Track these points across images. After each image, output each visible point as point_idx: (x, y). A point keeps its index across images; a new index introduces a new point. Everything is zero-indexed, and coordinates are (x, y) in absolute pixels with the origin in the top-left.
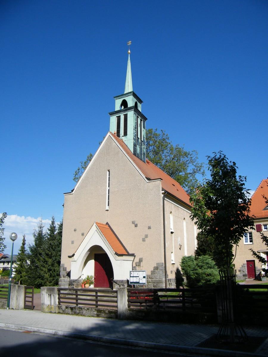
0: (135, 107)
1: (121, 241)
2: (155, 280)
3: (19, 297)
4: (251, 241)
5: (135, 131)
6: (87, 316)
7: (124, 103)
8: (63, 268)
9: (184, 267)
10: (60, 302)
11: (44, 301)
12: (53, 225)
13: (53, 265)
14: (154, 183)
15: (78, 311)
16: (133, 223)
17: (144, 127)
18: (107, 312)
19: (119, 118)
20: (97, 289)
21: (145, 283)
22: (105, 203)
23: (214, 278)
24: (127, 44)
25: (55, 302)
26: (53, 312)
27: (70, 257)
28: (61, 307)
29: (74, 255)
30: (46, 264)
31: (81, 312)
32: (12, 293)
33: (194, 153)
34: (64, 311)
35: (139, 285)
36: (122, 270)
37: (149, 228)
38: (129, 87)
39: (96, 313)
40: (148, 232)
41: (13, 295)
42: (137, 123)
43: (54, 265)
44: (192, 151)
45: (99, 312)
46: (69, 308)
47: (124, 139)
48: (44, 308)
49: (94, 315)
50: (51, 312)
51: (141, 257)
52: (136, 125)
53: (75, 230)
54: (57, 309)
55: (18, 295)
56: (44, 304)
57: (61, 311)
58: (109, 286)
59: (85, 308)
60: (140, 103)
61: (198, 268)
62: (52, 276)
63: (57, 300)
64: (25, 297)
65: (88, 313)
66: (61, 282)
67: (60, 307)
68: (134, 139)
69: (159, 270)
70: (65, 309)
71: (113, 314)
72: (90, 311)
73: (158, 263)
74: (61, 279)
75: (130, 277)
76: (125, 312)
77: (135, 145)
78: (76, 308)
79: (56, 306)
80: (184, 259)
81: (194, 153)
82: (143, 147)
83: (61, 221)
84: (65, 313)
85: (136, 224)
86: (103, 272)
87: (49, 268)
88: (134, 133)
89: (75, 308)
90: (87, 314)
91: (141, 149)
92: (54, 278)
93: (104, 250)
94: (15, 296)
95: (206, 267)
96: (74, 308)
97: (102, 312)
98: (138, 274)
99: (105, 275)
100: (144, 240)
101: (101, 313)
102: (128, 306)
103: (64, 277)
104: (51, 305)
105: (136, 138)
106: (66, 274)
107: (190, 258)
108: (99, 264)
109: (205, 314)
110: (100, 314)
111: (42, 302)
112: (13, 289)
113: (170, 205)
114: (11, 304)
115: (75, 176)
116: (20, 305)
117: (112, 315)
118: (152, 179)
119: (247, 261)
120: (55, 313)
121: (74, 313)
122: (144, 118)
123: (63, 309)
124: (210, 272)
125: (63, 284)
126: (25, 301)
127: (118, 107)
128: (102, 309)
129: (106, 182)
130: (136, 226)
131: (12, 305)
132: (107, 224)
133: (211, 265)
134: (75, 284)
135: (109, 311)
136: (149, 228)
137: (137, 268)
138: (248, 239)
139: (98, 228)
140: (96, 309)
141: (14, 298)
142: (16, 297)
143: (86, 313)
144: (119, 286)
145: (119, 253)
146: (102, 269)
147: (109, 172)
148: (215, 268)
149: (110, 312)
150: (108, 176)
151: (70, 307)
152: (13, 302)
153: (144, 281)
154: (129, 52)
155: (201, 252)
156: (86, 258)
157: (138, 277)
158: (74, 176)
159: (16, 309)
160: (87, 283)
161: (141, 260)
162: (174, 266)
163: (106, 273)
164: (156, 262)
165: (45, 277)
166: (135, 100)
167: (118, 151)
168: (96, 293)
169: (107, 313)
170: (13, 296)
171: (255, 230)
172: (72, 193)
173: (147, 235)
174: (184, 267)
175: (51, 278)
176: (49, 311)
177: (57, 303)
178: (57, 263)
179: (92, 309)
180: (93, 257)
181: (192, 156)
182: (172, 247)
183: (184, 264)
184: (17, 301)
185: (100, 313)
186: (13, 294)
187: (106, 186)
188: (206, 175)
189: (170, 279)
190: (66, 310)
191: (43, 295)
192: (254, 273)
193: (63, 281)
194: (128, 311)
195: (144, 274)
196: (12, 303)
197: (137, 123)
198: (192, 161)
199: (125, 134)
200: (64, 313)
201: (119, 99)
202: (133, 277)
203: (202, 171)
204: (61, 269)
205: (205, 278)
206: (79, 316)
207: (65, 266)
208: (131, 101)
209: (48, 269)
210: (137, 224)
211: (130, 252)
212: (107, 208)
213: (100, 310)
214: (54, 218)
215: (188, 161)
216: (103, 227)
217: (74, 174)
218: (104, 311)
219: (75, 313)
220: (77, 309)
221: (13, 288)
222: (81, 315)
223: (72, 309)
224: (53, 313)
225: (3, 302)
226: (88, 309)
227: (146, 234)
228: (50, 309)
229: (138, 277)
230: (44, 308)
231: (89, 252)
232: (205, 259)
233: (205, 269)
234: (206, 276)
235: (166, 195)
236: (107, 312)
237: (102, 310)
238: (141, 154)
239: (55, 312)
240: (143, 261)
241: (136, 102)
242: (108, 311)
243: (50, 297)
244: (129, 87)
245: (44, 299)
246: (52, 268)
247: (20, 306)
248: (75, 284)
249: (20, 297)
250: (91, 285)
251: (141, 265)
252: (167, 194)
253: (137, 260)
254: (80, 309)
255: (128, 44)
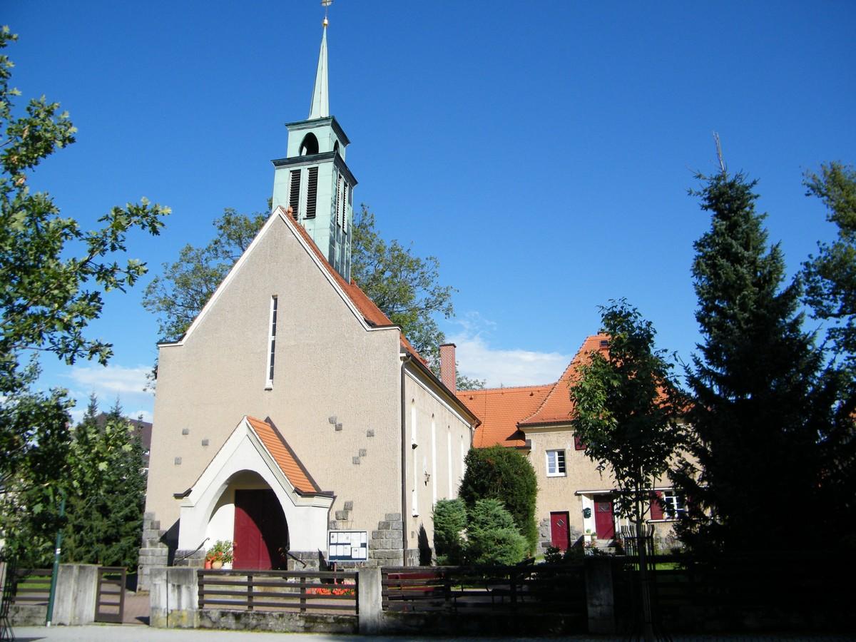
0: (335, 156)
1: (301, 463)
2: (382, 552)
3: (82, 593)
4: (562, 470)
5: (333, 210)
6: (281, 632)
7: (310, 143)
8: (150, 522)
9: (442, 523)
10: (201, 604)
11: (159, 600)
12: (92, 415)
13: (87, 515)
14: (383, 334)
15: (254, 622)
16: (331, 421)
17: (350, 202)
18: (331, 620)
19: (296, 176)
20: (236, 570)
21: (365, 559)
22: (265, 372)
23: (512, 548)
24: (322, 3)
25: (191, 603)
26: (186, 626)
27: (178, 496)
28: (208, 614)
29: (188, 493)
30: (71, 513)
31: (261, 622)
32: (60, 584)
33: (430, 264)
34: (214, 623)
35: (343, 564)
36: (307, 530)
37: (370, 434)
38: (321, 108)
39: (302, 623)
40: (367, 443)
41: (62, 591)
42: (337, 191)
43: (91, 514)
44: (427, 259)
45: (310, 622)
46: (230, 614)
47: (307, 224)
48: (158, 619)
49: (297, 629)
50: (179, 627)
51: (349, 500)
52: (335, 196)
53: (185, 433)
54: (195, 620)
55: (78, 588)
56: (157, 608)
57: (208, 624)
58: (270, 566)
59: (274, 614)
60: (343, 143)
61: (477, 526)
62: (84, 543)
63: (196, 598)
64: (99, 593)
65: (283, 623)
66: (144, 557)
67: (204, 614)
68: (331, 227)
69: (391, 530)
70: (219, 619)
71: (346, 626)
72: (287, 620)
73: (388, 513)
74: (145, 550)
75: (330, 544)
76: (377, 619)
77: (332, 243)
78: (248, 615)
79: (195, 611)
80: (443, 506)
81: (430, 264)
82: (346, 246)
83: (114, 407)
84: (218, 628)
85: (337, 423)
86: (255, 533)
87: (76, 523)
88: (332, 215)
89: (246, 614)
90: (277, 626)
91: (343, 250)
92: (91, 549)
93: (266, 483)
94: (71, 594)
95: (496, 524)
96: (243, 616)
97: (319, 620)
98: (347, 538)
99: (261, 539)
100: (356, 462)
101: (316, 624)
102: (383, 606)
103: (152, 544)
104: (179, 610)
105: (335, 227)
106: (158, 539)
107: (455, 504)
108: (247, 516)
109: (561, 615)
110: (313, 627)
111: (152, 604)
112: (64, 575)
113: (414, 385)
114: (58, 613)
115: (147, 295)
116: (85, 613)
117: (344, 626)
118: (378, 324)
119: (552, 513)
120: (192, 628)
121: (242, 627)
122: (351, 181)
123: (213, 619)
124: (504, 535)
125: (149, 562)
126: (98, 604)
127: (293, 149)
128: (319, 616)
129: (268, 324)
130: (339, 428)
131: (60, 614)
132: (268, 420)
133: (503, 520)
134: (190, 560)
135: (337, 618)
136: (370, 434)
137: (340, 524)
138: (555, 466)
139: (253, 430)
140: (302, 614)
141: (65, 599)
142: (73, 595)
143: (276, 625)
144: (303, 565)
145: (182, 492)
146: (254, 525)
147: (276, 300)
148: (512, 528)
149: (339, 621)
150: (272, 311)
151: (233, 613)
152: (64, 608)
153: (363, 553)
154: (326, 22)
155: (476, 490)
156: (217, 500)
157: (350, 544)
158: (144, 295)
159: (70, 625)
160: (217, 559)
161: (348, 507)
162: (416, 521)
163: (263, 534)
164: (385, 512)
165: (67, 546)
166: (335, 137)
167: (300, 254)
168: (303, 579)
169: (332, 623)
170: (64, 592)
171: (508, 439)
172: (179, 344)
173: (365, 450)
174: (442, 523)
175: (83, 549)
176: (174, 623)
177: (196, 605)
178: (97, 511)
179: (291, 615)
180: (233, 497)
181: (425, 269)
182: (414, 479)
183: (444, 516)
184: (76, 603)
185: (312, 624)
186: (63, 587)
187: (268, 333)
188: (454, 315)
189: (411, 550)
190: (223, 619)
191: (157, 588)
192: (567, 540)
193: (150, 554)
194: (385, 617)
195: (364, 538)
196: (60, 610)
197: (337, 191)
198: (425, 283)
199: (311, 214)
200: (214, 627)
201: (299, 129)
202: (337, 544)
203: (445, 305)
204: (147, 526)
205: (493, 548)
206: (259, 632)
207: (157, 519)
208: (326, 138)
209: (74, 526)
210: (341, 425)
211: (324, 489)
212: (269, 384)
213: (313, 617)
214: (95, 397)
215: (415, 279)
216: (261, 429)
217: (143, 292)
218: (322, 618)
219: (245, 627)
220: (251, 617)
221: (63, 572)
222: (264, 630)
223: (237, 617)
224: (184, 628)
225: (31, 610)
226: (281, 616)
227: (363, 448)
228: (178, 620)
229: (350, 544)
230: (158, 619)
231: (226, 486)
232: (491, 506)
233: (491, 528)
234: (495, 544)
235: (409, 362)
236: (331, 620)
237: (317, 618)
238: (342, 263)
239: (190, 625)
240: (354, 508)
241: (337, 141)
242: (334, 618)
243: (176, 591)
244: (321, 108)
245: (159, 597)
246: (86, 523)
247: (84, 617)
248: (190, 560)
249: (85, 592)
250: (225, 564)
251: (350, 519)
252: (412, 360)
253: (339, 506)
254: (260, 616)
255: (324, 4)
